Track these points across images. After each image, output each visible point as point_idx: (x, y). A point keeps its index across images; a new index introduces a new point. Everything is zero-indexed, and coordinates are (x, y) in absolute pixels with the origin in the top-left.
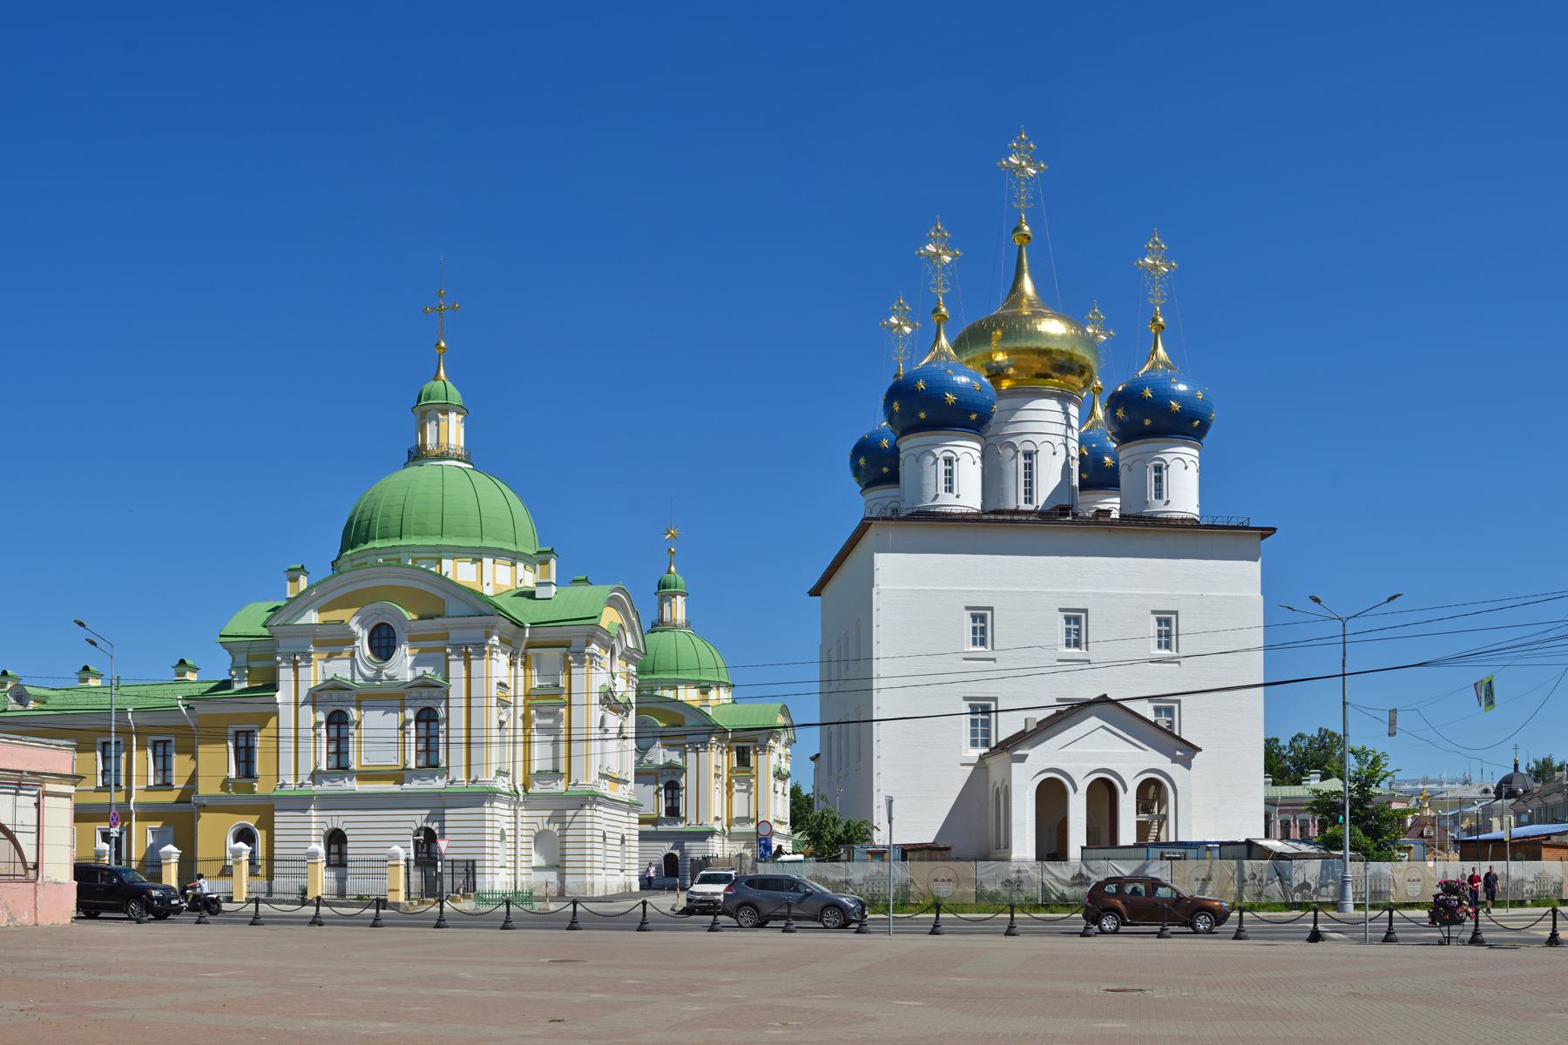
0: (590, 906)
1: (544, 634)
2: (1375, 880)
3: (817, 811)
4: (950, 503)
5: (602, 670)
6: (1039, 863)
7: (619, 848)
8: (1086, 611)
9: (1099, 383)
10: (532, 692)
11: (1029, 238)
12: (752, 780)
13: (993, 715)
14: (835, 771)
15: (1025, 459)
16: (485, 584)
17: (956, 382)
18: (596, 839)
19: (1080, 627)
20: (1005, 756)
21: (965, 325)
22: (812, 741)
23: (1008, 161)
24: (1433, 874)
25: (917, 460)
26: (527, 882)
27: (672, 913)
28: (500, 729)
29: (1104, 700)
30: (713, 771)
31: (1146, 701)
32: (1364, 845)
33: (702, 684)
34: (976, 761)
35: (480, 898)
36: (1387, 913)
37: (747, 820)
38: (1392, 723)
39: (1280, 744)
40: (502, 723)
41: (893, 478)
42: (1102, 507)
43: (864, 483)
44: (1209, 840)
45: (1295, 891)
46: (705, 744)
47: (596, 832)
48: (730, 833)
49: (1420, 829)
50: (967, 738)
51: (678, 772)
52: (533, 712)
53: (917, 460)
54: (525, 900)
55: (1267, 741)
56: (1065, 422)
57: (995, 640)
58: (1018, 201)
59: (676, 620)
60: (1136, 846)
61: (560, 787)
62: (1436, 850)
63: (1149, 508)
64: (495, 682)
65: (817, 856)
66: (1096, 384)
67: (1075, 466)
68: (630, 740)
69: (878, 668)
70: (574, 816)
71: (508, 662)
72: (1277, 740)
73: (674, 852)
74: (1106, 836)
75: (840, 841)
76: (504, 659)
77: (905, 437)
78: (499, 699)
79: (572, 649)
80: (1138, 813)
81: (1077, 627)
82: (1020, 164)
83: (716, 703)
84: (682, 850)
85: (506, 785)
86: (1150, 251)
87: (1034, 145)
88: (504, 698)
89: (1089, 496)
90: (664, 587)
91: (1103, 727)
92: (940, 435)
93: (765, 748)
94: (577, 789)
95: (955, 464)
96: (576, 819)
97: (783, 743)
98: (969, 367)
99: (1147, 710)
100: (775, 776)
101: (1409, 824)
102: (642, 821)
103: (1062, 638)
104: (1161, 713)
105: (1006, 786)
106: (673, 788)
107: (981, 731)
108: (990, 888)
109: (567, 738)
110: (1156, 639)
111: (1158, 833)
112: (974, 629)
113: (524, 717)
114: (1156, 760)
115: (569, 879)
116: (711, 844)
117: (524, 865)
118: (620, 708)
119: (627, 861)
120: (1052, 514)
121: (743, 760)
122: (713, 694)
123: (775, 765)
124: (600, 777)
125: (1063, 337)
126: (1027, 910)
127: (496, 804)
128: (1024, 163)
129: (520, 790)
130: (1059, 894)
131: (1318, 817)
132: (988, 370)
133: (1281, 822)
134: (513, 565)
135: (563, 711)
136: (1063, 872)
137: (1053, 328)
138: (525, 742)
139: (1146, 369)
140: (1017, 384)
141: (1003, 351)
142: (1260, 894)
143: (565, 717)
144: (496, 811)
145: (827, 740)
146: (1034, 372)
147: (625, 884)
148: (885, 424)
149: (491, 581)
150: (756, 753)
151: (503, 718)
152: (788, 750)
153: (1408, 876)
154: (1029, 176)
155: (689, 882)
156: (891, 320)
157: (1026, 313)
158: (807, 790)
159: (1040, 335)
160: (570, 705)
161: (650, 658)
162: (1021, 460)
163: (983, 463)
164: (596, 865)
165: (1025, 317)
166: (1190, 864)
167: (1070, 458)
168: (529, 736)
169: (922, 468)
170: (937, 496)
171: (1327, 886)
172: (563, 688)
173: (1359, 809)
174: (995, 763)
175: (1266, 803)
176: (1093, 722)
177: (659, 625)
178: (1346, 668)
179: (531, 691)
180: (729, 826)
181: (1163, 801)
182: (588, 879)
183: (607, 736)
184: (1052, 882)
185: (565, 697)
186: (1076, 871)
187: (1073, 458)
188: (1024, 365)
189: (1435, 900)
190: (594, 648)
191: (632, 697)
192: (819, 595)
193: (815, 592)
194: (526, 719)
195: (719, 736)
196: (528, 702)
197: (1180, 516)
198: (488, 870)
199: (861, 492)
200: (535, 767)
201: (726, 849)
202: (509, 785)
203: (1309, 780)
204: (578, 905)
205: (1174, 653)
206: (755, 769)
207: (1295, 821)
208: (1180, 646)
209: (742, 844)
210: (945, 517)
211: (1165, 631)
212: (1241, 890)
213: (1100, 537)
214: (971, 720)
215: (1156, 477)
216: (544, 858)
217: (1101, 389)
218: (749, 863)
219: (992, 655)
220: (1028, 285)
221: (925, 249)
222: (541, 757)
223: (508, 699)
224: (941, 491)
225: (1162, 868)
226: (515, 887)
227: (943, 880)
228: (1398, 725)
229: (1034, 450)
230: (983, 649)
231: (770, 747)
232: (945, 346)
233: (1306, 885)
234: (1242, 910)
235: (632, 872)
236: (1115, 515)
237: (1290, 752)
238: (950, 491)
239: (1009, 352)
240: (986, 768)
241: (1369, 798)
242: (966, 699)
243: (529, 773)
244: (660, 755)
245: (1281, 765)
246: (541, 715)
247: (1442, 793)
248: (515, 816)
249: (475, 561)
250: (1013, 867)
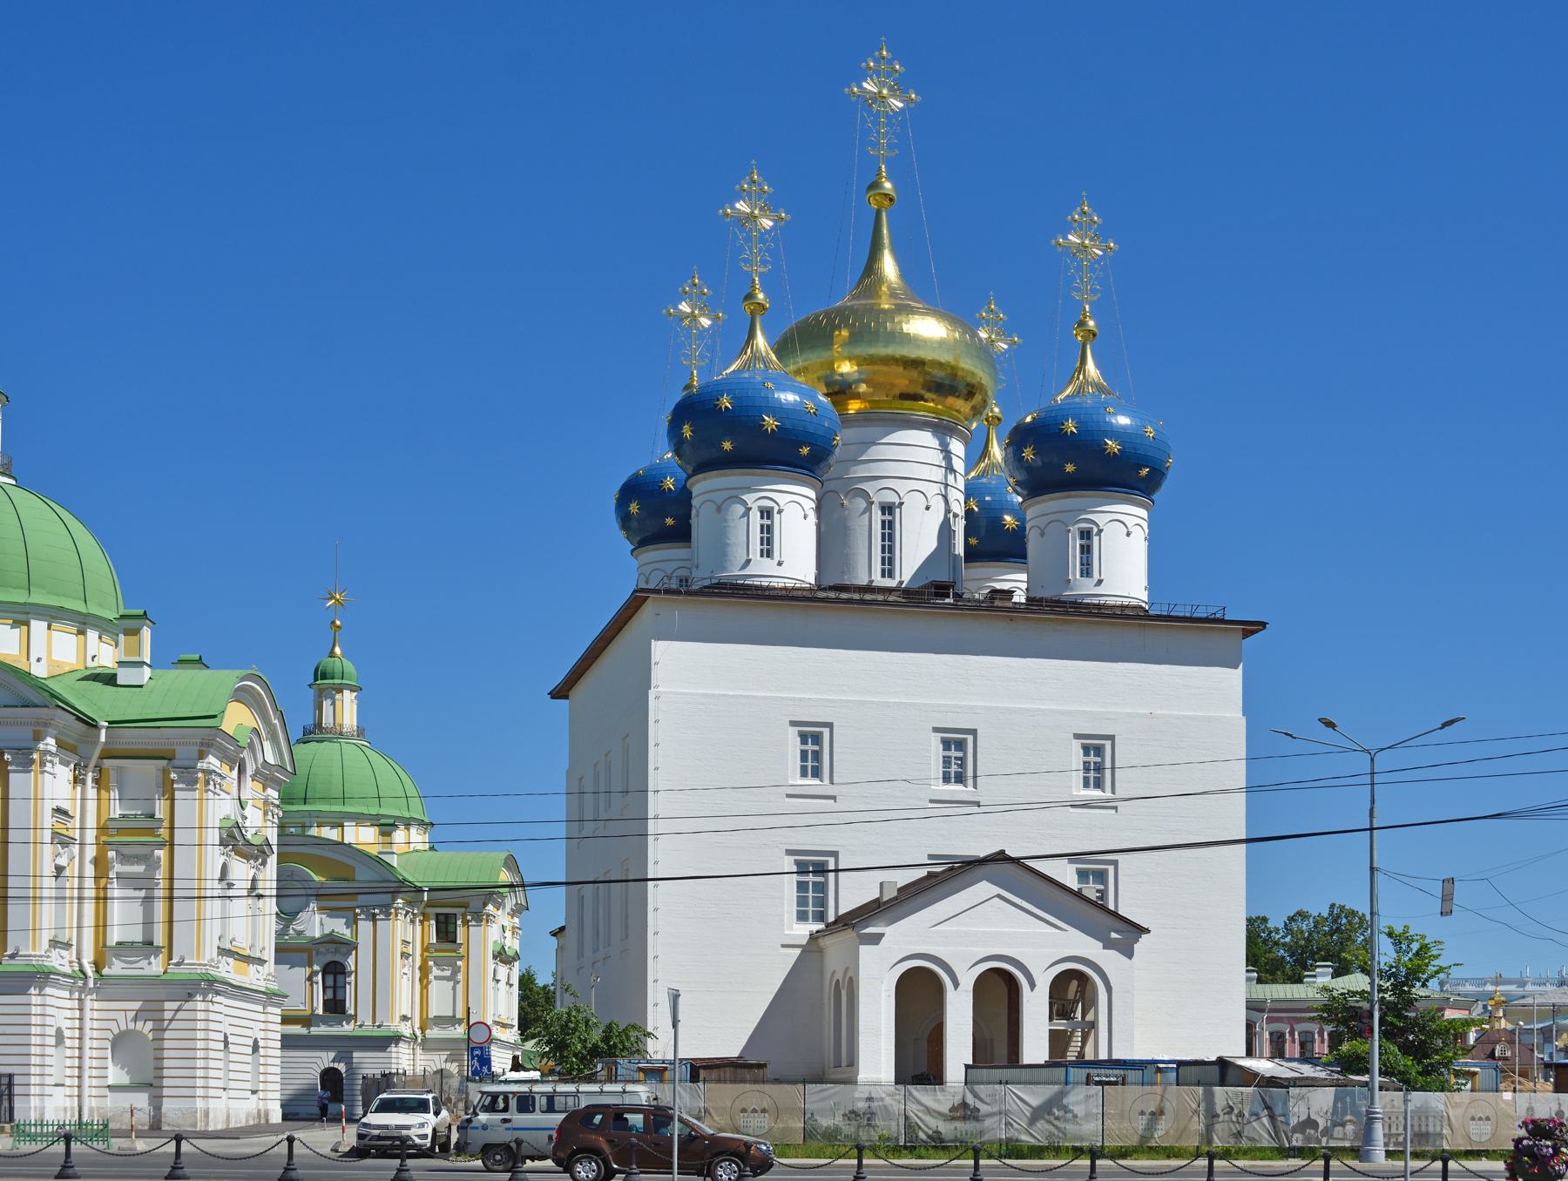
0: (205, 1144)
1: (131, 738)
2: (1420, 1118)
3: (560, 1008)
4: (765, 572)
5: (223, 795)
6: (901, 1087)
7: (249, 1059)
8: (974, 732)
9: (996, 410)
10: (111, 825)
11: (891, 200)
12: (459, 963)
13: (831, 876)
14: (588, 952)
15: (883, 514)
16: (33, 659)
17: (779, 400)
18: (212, 1045)
19: (965, 754)
20: (849, 935)
21: (794, 319)
22: (553, 907)
23: (860, 87)
24: (1510, 1111)
25: (719, 509)
26: (98, 1108)
27: (333, 1155)
28: (57, 877)
29: (1000, 857)
30: (399, 948)
31: (1065, 861)
32: (1402, 1068)
33: (383, 821)
34: (804, 942)
35: (20, 1132)
36: (1438, 1165)
37: (452, 1021)
38: (1447, 898)
39: (1271, 925)
40: (59, 870)
41: (682, 534)
42: (998, 586)
43: (638, 539)
44: (1161, 1058)
45: (1294, 1130)
46: (386, 909)
47: (212, 1035)
48: (425, 1040)
49: (1491, 1046)
50: (791, 907)
51: (344, 949)
52: (112, 854)
53: (719, 509)
54: (96, 1135)
55: (1250, 921)
56: (943, 464)
57: (835, 770)
58: (876, 145)
59: (341, 726)
60: (1047, 1065)
61: (156, 966)
62: (1517, 1078)
63: (1072, 590)
64: (48, 807)
65: (559, 1073)
66: (992, 411)
67: (959, 527)
68: (268, 900)
69: (655, 805)
70: (177, 1011)
71: (71, 778)
72: (1265, 920)
73: (336, 1065)
74: (1002, 1050)
75: (595, 1052)
76: (64, 773)
77: (700, 476)
78: (55, 834)
79: (176, 762)
80: (1051, 1019)
81: (960, 754)
82: (880, 92)
83: (404, 848)
84: (349, 1063)
85: (65, 962)
86: (1076, 225)
87: (901, 66)
88: (64, 832)
89: (980, 570)
90: (324, 677)
91: (999, 896)
92: (754, 475)
93: (480, 917)
94: (183, 970)
95: (776, 516)
96: (180, 1015)
97: (508, 909)
98: (799, 379)
99: (1066, 874)
100: (495, 957)
101: (1472, 1042)
102: (286, 1020)
103: (937, 769)
104: (1088, 877)
105: (851, 979)
106: (335, 972)
107: (812, 897)
108: (825, 1122)
109: (167, 893)
110: (1081, 774)
111: (1083, 1047)
112: (804, 755)
113: (96, 861)
114: (1080, 945)
115: (167, 1105)
116: (394, 1055)
117: (94, 1082)
118: (256, 853)
119: (262, 1078)
120: (923, 593)
121: (446, 932)
122: (399, 835)
123: (495, 942)
124: (219, 954)
125: (942, 343)
126: (882, 1154)
127: (48, 990)
128: (885, 91)
129: (89, 970)
130: (930, 1132)
131: (1328, 1028)
132: (828, 385)
133: (1271, 1034)
134: (81, 632)
135: (161, 854)
136: (937, 1101)
137: (927, 329)
138: (97, 898)
139: (1068, 392)
140: (871, 408)
141: (850, 359)
142: (1239, 1135)
143: (164, 863)
144: (49, 1001)
145: (576, 908)
146: (897, 391)
147: (259, 1111)
148: (670, 455)
149: (43, 656)
150: (466, 923)
151: (62, 861)
152: (516, 920)
153: (1472, 1112)
154: (892, 110)
155: (360, 1111)
156: (680, 307)
157: (887, 307)
158: (543, 979)
159: (908, 339)
160: (172, 845)
161: (300, 780)
162: (877, 516)
163: (819, 517)
164: (212, 1083)
165: (885, 312)
166: (1132, 1091)
167: (951, 515)
168: (105, 888)
169: (726, 521)
170: (748, 561)
171: (1343, 1125)
172: (161, 820)
173: (1395, 1016)
174: (834, 945)
175: (1248, 1008)
176: (984, 889)
177: (315, 732)
178: (1375, 820)
179: (108, 823)
180: (423, 1029)
181: (1090, 1002)
182: (200, 1104)
183: (231, 893)
184: (920, 1114)
185: (164, 833)
186: (958, 1100)
187: (956, 516)
188: (881, 380)
189: (1516, 1147)
190: (212, 762)
191: (272, 835)
192: (566, 697)
193: (560, 693)
194: (100, 863)
195: (409, 896)
196: (103, 838)
197: (1119, 601)
198: (33, 1090)
199: (632, 551)
200: (115, 936)
201: (418, 1062)
202: (71, 962)
203: (1314, 976)
204: (183, 1143)
205: (1108, 794)
206: (129, 1020)
207: (1292, 1033)
208: (1117, 785)
209: (444, 1055)
210: (760, 592)
211: (1095, 763)
212: (1209, 1129)
213: (996, 628)
214: (798, 882)
215: (1082, 546)
216: (128, 1073)
217: (999, 419)
218: (455, 1083)
219: (830, 791)
220: (889, 267)
221: (733, 208)
222: (124, 921)
223: (70, 833)
224: (755, 553)
225: (1088, 1097)
226: (80, 1115)
227: (754, 1111)
228: (1455, 901)
229: (897, 501)
230: (816, 782)
231: (488, 915)
232: (763, 349)
233: (1310, 1123)
234: (1211, 1157)
235: (270, 1095)
236: (1020, 597)
237: (1283, 937)
238: (768, 556)
239: (861, 361)
240: (821, 951)
241: (1410, 1003)
242: (789, 852)
243: (105, 945)
244: (315, 923)
245: (1271, 956)
246: (125, 859)
247: (1524, 997)
248: (81, 1010)
249: (17, 624)
250: (860, 1092)
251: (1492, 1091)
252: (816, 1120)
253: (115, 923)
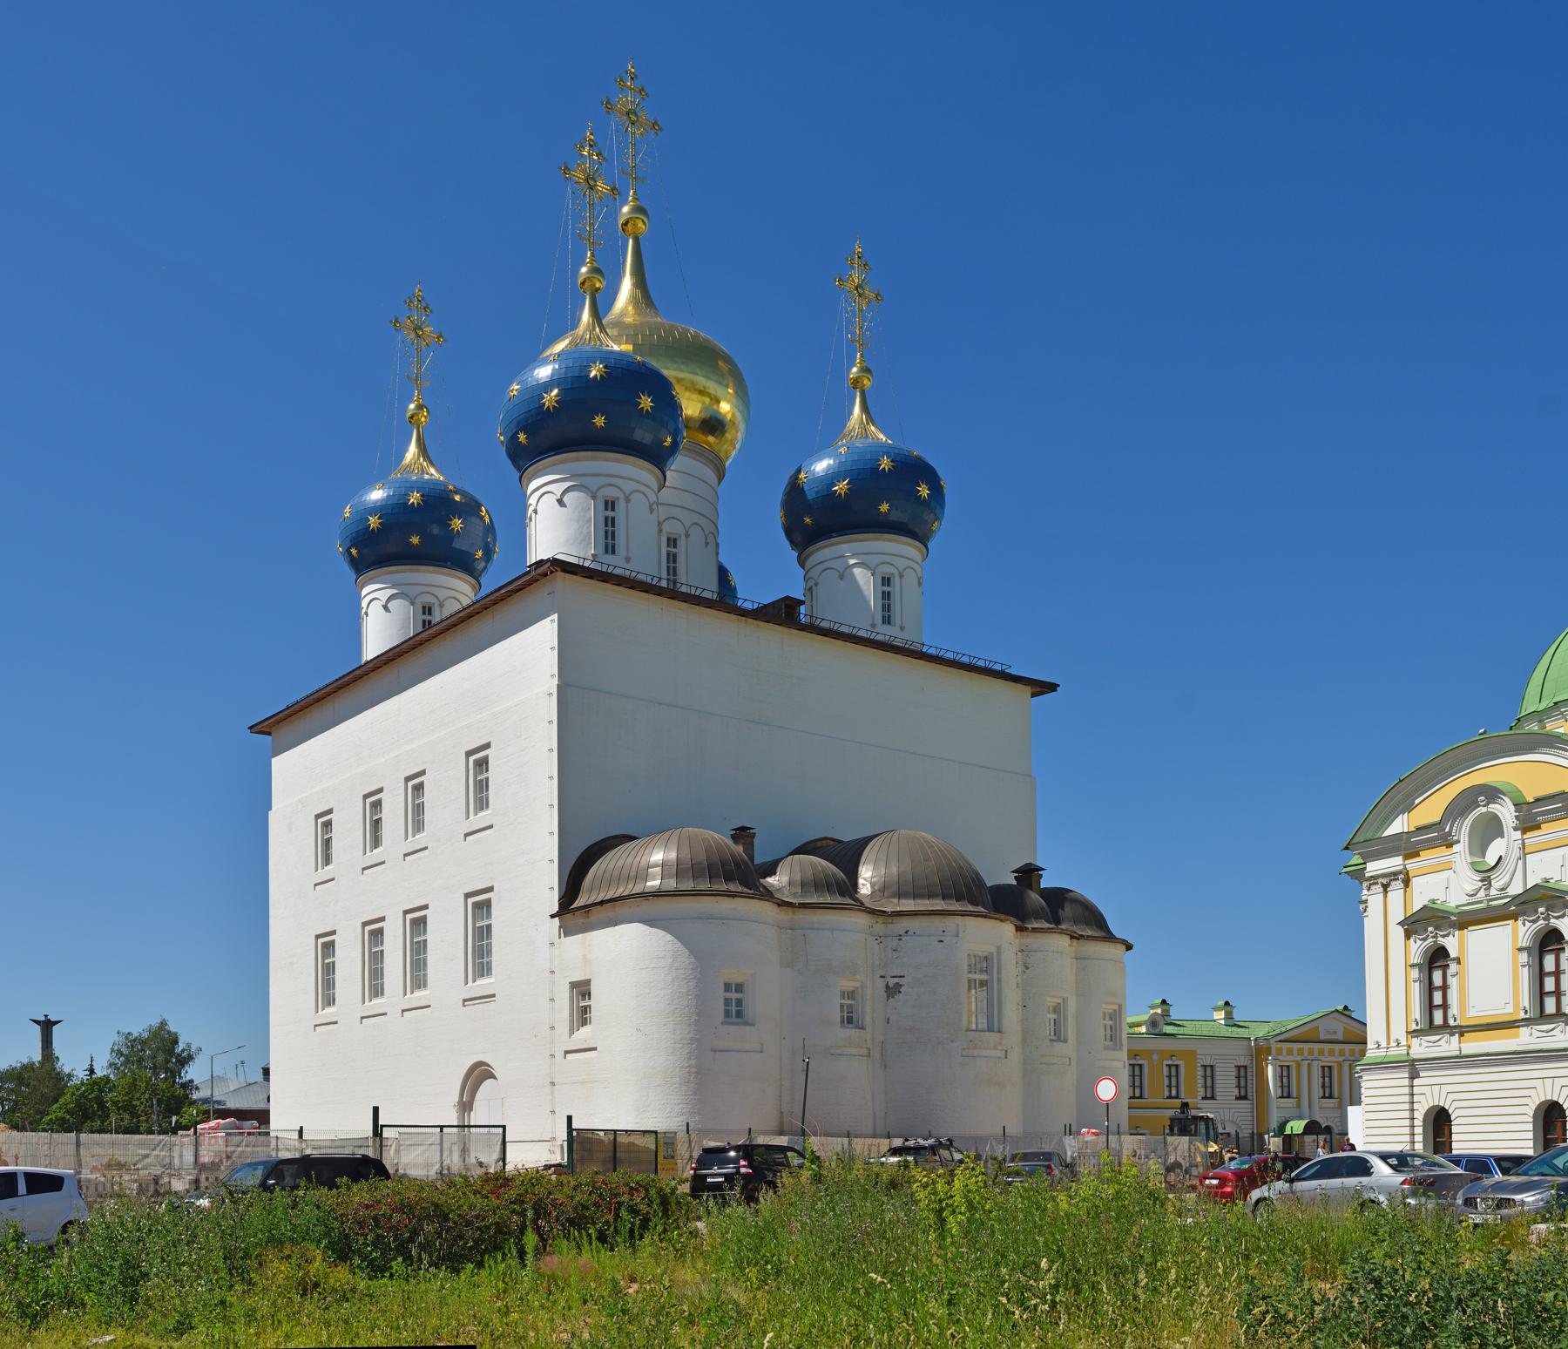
55: (269, 1081)
65: (432, 1260)
251: (1527, 1022)
252: (642, 1237)
253: (1462, 1045)
